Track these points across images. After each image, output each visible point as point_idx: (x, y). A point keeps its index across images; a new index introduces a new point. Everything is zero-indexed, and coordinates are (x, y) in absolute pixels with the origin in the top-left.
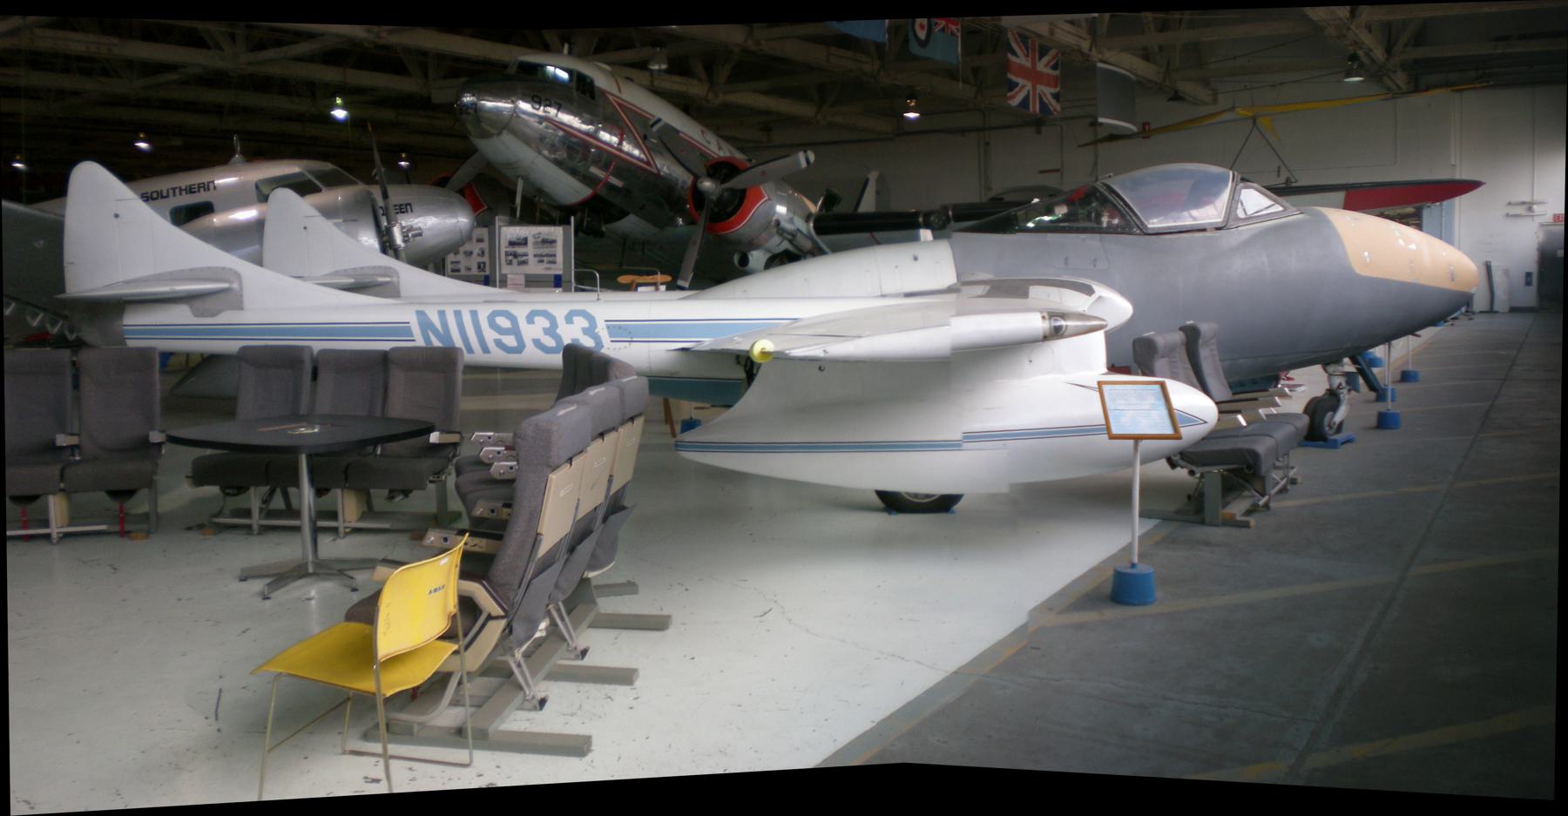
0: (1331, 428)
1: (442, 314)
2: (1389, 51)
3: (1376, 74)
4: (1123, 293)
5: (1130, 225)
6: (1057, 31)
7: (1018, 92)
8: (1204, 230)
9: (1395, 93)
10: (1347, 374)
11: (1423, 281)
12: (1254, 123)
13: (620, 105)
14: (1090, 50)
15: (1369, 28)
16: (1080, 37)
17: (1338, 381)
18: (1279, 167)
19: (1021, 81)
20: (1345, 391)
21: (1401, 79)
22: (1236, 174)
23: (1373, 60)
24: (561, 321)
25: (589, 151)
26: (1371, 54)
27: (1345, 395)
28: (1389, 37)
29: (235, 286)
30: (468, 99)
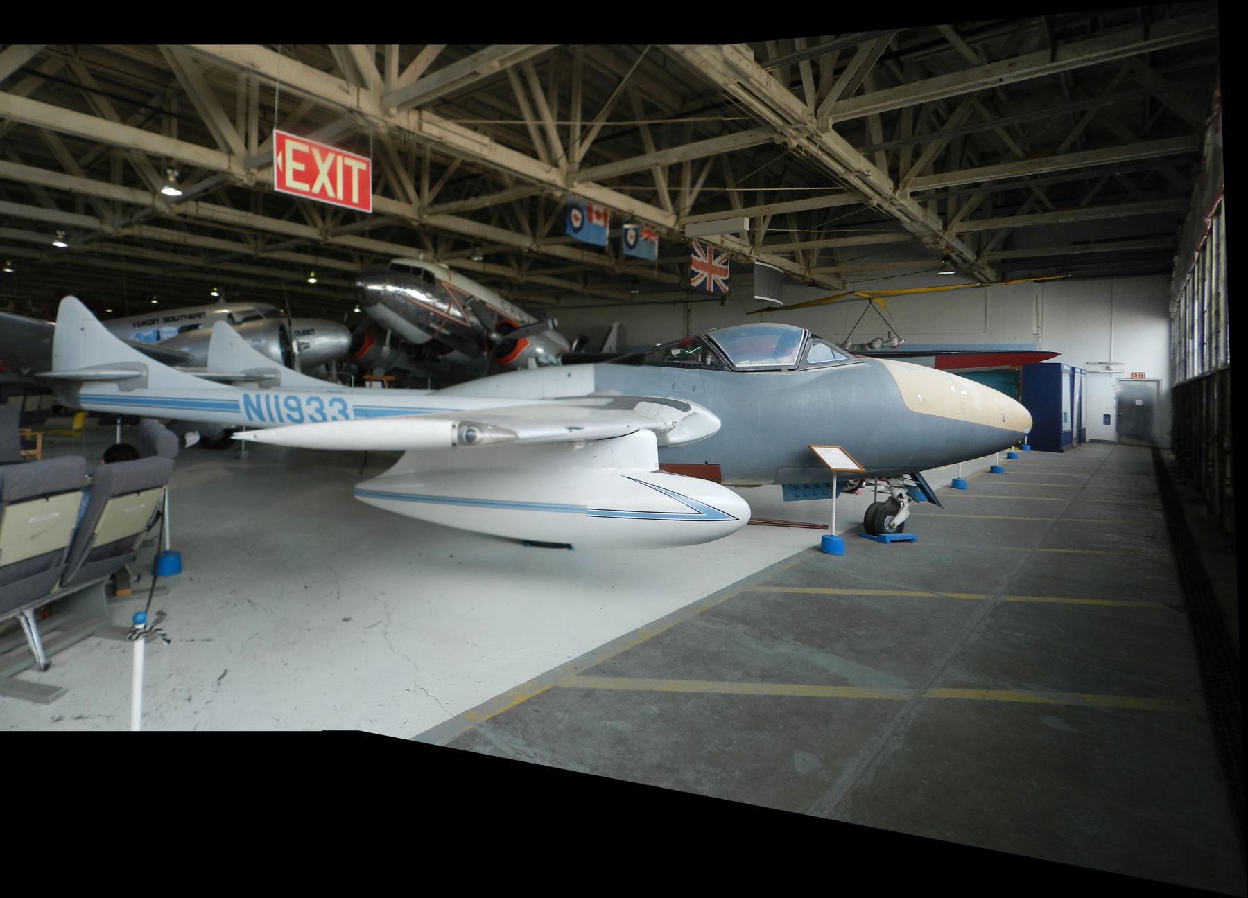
0: (891, 528)
1: (258, 397)
2: (978, 253)
3: (966, 272)
4: (715, 411)
5: (721, 364)
6: (725, 241)
7: (698, 278)
8: (780, 371)
9: (984, 283)
10: (907, 487)
11: (972, 420)
12: (870, 302)
13: (450, 288)
14: (750, 254)
15: (960, 237)
16: (743, 246)
17: (897, 492)
18: (889, 332)
19: (700, 271)
20: (905, 500)
21: (990, 273)
22: (808, 331)
23: (965, 261)
24: (326, 404)
25: (429, 314)
26: (962, 255)
27: (905, 504)
28: (978, 242)
29: (144, 374)
30: (359, 284)
